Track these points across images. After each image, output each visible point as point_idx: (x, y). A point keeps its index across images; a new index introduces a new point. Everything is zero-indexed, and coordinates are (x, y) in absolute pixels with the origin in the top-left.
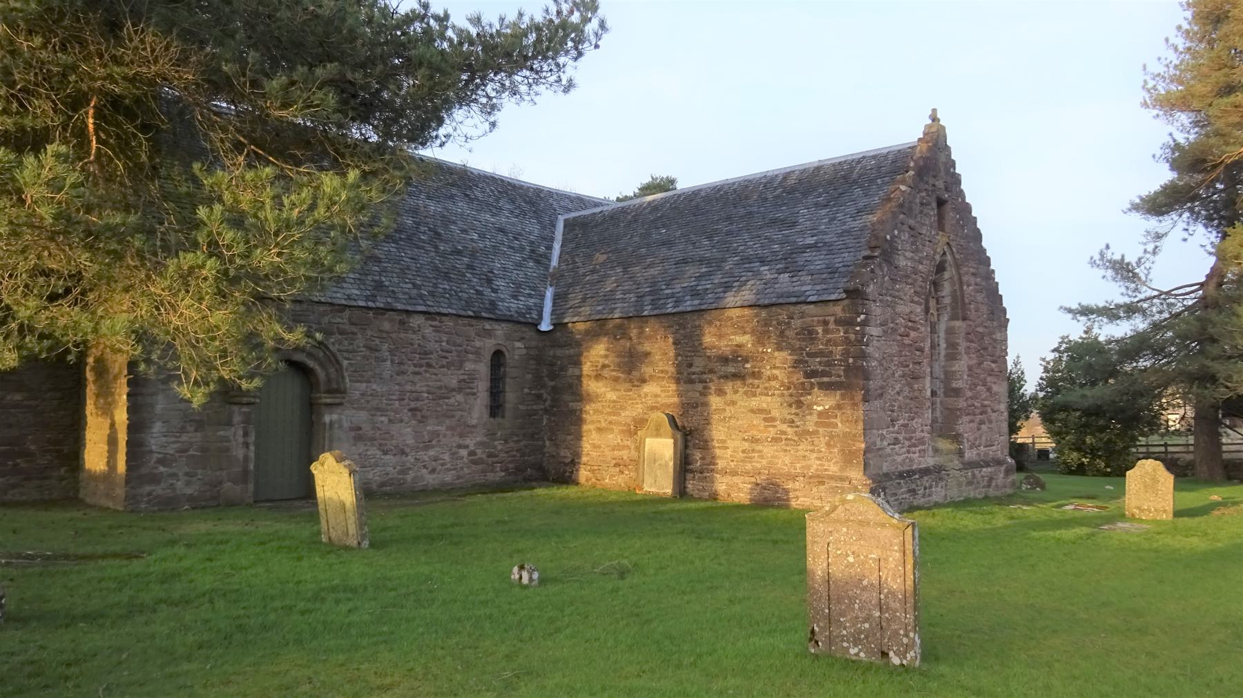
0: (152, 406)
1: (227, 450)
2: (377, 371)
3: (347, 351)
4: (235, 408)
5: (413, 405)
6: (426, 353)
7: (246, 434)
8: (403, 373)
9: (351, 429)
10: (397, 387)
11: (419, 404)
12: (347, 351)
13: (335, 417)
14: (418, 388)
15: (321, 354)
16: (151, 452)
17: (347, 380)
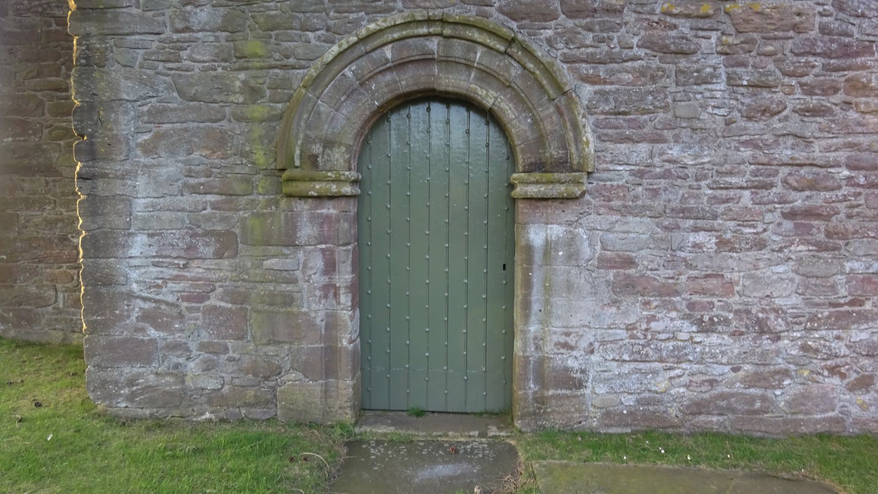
0: (127, 201)
1: (288, 300)
2: (683, 109)
3: (590, 60)
4: (303, 207)
5: (799, 200)
6: (847, 52)
7: (330, 267)
8: (767, 112)
9: (605, 263)
10: (747, 153)
11: (819, 199)
12: (590, 60)
13: (557, 231)
14: (817, 152)
15: (515, 71)
16: (131, 296)
17: (589, 135)
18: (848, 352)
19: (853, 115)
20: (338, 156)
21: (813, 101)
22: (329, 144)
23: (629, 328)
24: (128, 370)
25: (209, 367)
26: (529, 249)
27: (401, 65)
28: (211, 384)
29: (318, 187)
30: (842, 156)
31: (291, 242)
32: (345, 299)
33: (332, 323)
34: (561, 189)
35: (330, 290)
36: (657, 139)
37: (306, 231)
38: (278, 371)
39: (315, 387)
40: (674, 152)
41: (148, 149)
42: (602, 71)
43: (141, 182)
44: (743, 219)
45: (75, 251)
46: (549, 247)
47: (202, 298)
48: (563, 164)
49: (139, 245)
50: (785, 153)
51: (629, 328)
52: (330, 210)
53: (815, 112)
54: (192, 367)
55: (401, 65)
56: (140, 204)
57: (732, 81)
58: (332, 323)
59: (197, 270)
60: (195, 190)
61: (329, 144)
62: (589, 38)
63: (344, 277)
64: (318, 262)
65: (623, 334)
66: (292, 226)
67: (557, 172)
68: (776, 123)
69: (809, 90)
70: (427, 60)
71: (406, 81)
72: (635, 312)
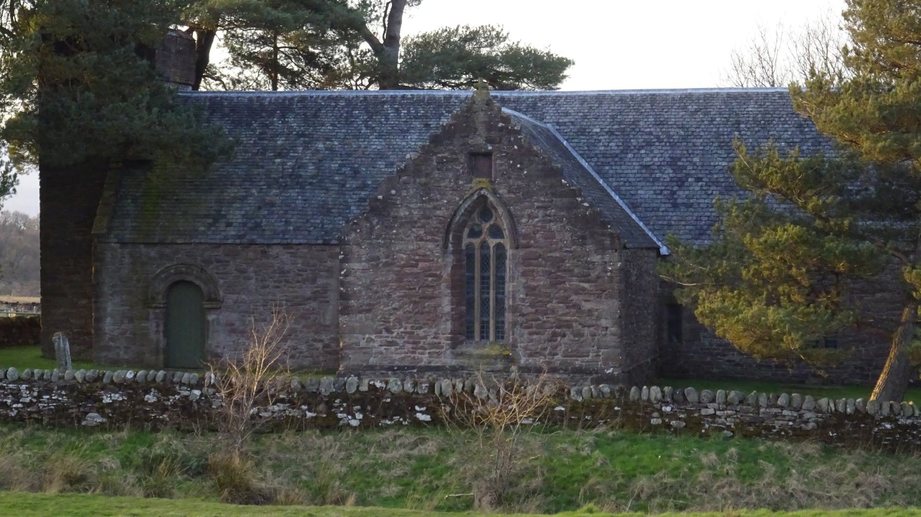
4: (151, 311)
7: (158, 326)
9: (227, 325)
10: (261, 297)
16: (106, 333)
18: (11, 29)
19: (286, 288)
20: (160, 297)
21: (276, 284)
22: (158, 294)
23: (234, 342)
24: (104, 354)
25: (125, 353)
26: (208, 321)
27: (175, 274)
28: (126, 357)
29: (154, 305)
30: (285, 298)
31: (147, 319)
32: (161, 334)
33: (158, 341)
34: (214, 306)
35: (157, 332)
36: (239, 294)
37: (152, 316)
38: (144, 354)
39: (154, 358)
40: (243, 297)
41: (111, 295)
42: (225, 276)
43: (109, 303)
44: (261, 314)
45: (14, 330)
46: (213, 321)
47: (124, 334)
48: (216, 300)
49: (109, 320)
50: (270, 297)
51: (234, 342)
52: (158, 311)
53: (277, 287)
54: (122, 353)
55: (175, 274)
56: (109, 309)
57: (257, 279)
58: (158, 341)
59: (123, 327)
60: (123, 305)
61: (158, 294)
62: (221, 268)
63: (161, 328)
64: (154, 325)
65: (232, 343)
66: (149, 314)
67: (99, 320)
68: (267, 290)
69: (275, 282)
70: (182, 273)
71: (177, 278)
72: (234, 337)
